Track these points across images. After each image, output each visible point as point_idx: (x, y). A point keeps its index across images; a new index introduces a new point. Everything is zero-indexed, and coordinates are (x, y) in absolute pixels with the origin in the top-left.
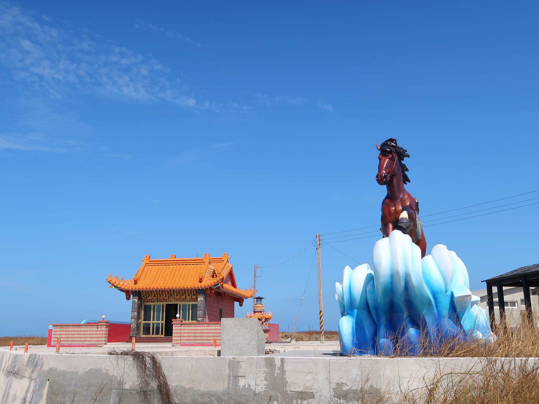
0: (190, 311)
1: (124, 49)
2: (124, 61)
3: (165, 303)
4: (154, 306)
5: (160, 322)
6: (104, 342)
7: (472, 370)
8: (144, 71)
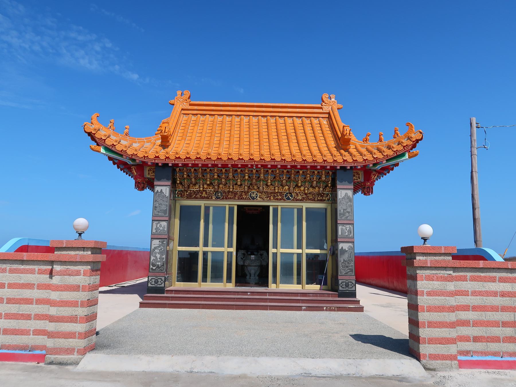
0: (304, 224)
1: (81, 28)
2: (81, 38)
3: (236, 203)
4: (207, 208)
5: (225, 249)
6: (81, 343)
7: (153, 248)
8: (97, 48)
